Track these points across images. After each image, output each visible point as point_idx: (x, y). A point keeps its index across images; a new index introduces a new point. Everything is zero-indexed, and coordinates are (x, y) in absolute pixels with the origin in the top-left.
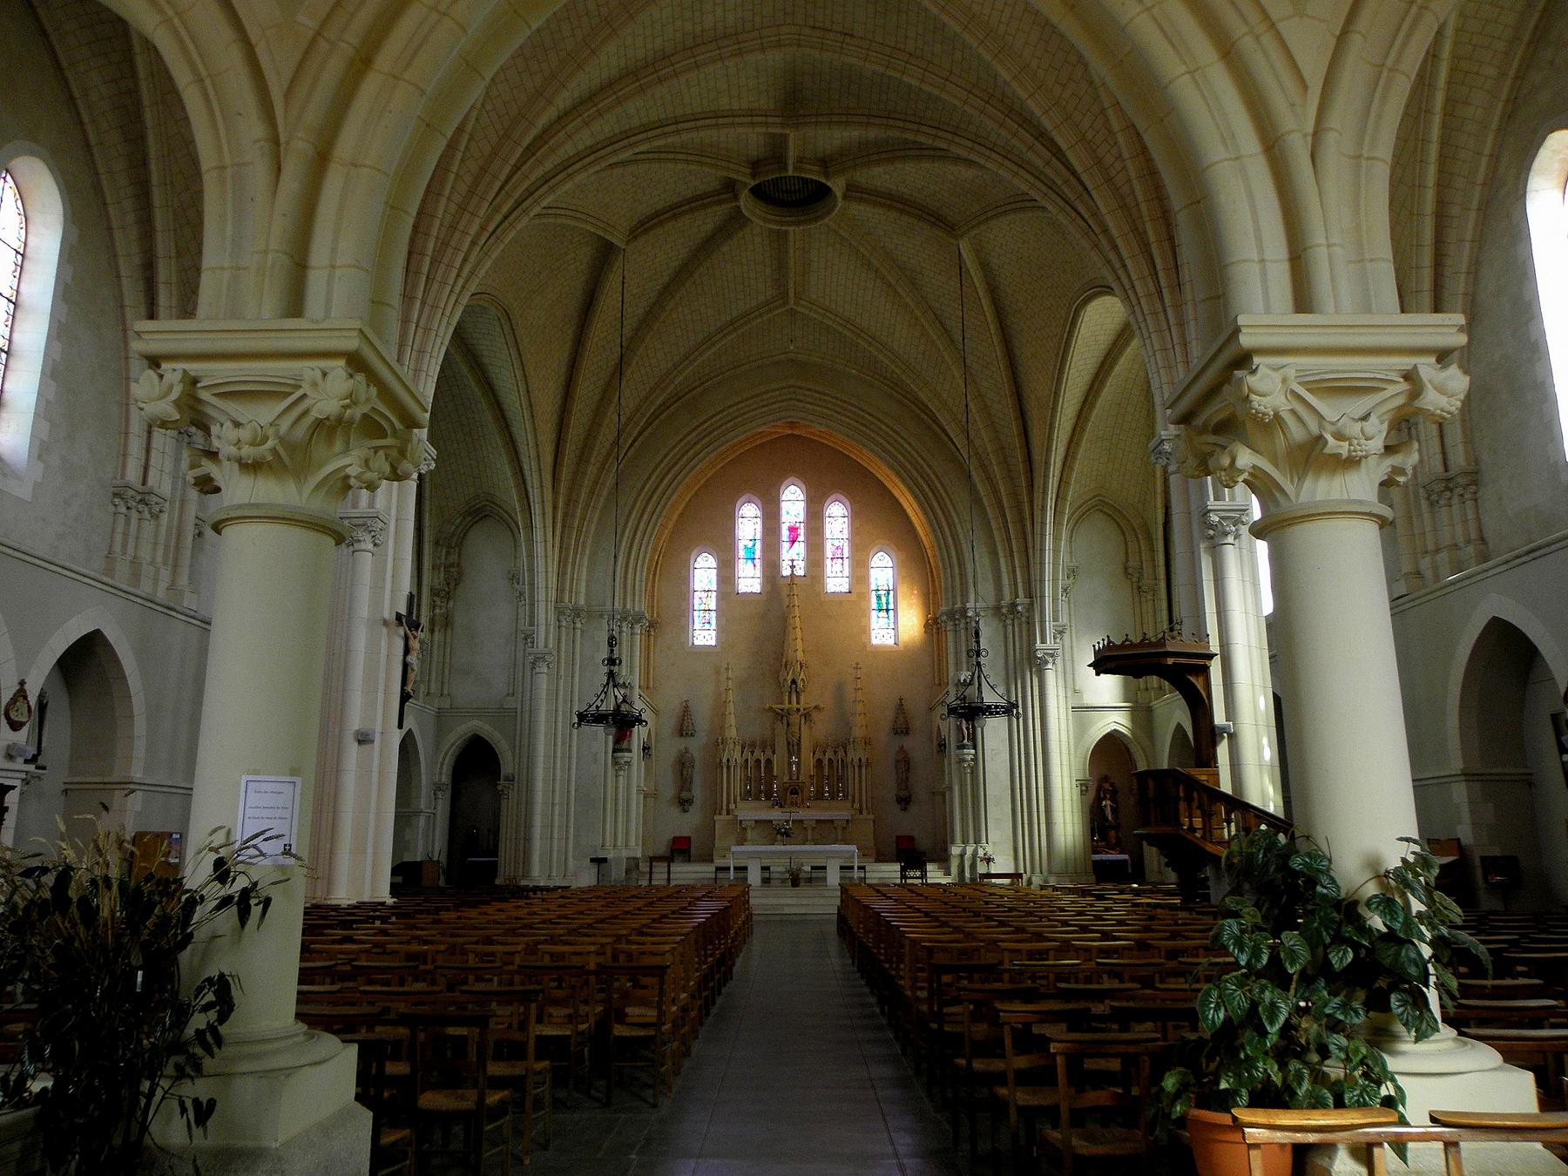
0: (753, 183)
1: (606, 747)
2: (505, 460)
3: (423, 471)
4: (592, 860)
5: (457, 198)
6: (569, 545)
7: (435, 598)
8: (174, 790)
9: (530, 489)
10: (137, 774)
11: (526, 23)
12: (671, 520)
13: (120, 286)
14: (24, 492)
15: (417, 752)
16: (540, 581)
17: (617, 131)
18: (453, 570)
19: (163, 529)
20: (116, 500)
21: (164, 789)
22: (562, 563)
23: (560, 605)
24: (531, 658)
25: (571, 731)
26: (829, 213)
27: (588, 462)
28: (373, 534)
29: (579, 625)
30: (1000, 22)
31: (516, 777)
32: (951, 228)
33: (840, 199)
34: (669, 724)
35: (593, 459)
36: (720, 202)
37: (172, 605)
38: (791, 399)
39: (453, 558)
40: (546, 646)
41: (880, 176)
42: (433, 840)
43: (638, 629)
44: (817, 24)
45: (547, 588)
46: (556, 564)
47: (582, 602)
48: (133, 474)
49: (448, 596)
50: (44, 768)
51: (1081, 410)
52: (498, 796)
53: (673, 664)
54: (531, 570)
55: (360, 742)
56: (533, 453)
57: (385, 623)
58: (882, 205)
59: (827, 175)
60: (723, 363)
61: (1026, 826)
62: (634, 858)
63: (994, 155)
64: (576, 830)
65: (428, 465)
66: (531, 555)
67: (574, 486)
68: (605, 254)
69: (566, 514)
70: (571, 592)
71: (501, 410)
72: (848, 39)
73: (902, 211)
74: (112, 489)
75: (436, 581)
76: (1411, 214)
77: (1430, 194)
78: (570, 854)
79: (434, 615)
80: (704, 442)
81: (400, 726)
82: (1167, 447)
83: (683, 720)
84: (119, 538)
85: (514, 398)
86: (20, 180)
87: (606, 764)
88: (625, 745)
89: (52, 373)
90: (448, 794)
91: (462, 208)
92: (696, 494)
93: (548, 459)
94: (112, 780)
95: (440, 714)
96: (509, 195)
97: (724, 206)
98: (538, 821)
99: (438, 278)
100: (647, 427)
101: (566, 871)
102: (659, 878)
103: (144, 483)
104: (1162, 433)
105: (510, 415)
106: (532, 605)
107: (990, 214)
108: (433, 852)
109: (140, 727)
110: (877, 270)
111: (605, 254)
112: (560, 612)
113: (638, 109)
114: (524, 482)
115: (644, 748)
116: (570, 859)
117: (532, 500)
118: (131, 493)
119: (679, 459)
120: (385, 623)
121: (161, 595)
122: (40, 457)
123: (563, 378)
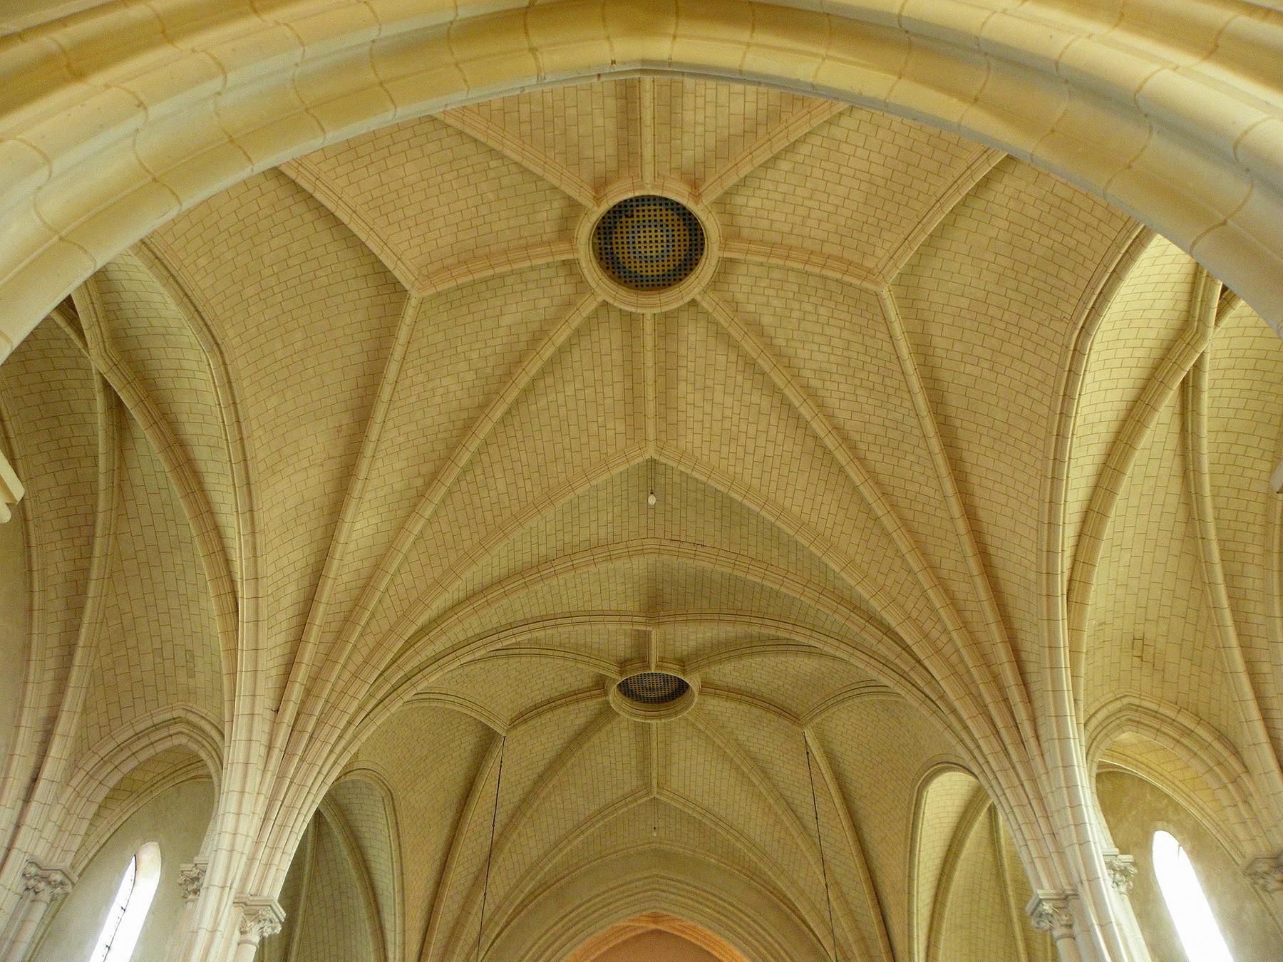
0: (621, 680)
2: (371, 947)
3: (266, 935)
5: (352, 667)
11: (320, 124)
12: (498, 925)
13: (16, 735)
17: (504, 623)
26: (687, 708)
30: (826, 527)
32: (796, 718)
33: (696, 694)
36: (591, 697)
38: (653, 889)
41: (728, 672)
44: (674, 538)
51: (936, 895)
56: (399, 940)
58: (733, 699)
59: (684, 672)
60: (592, 853)
63: (830, 641)
65: (273, 929)
68: (488, 740)
71: (375, 895)
72: (699, 548)
73: (751, 704)
76: (1224, 672)
77: (1237, 654)
82: (1047, 907)
85: (388, 881)
91: (355, 676)
96: (400, 668)
97: (595, 701)
99: (322, 737)
100: (514, 917)
104: (1039, 892)
107: (830, 703)
110: (732, 761)
111: (488, 740)
113: (522, 603)
119: (544, 951)
123: (438, 863)
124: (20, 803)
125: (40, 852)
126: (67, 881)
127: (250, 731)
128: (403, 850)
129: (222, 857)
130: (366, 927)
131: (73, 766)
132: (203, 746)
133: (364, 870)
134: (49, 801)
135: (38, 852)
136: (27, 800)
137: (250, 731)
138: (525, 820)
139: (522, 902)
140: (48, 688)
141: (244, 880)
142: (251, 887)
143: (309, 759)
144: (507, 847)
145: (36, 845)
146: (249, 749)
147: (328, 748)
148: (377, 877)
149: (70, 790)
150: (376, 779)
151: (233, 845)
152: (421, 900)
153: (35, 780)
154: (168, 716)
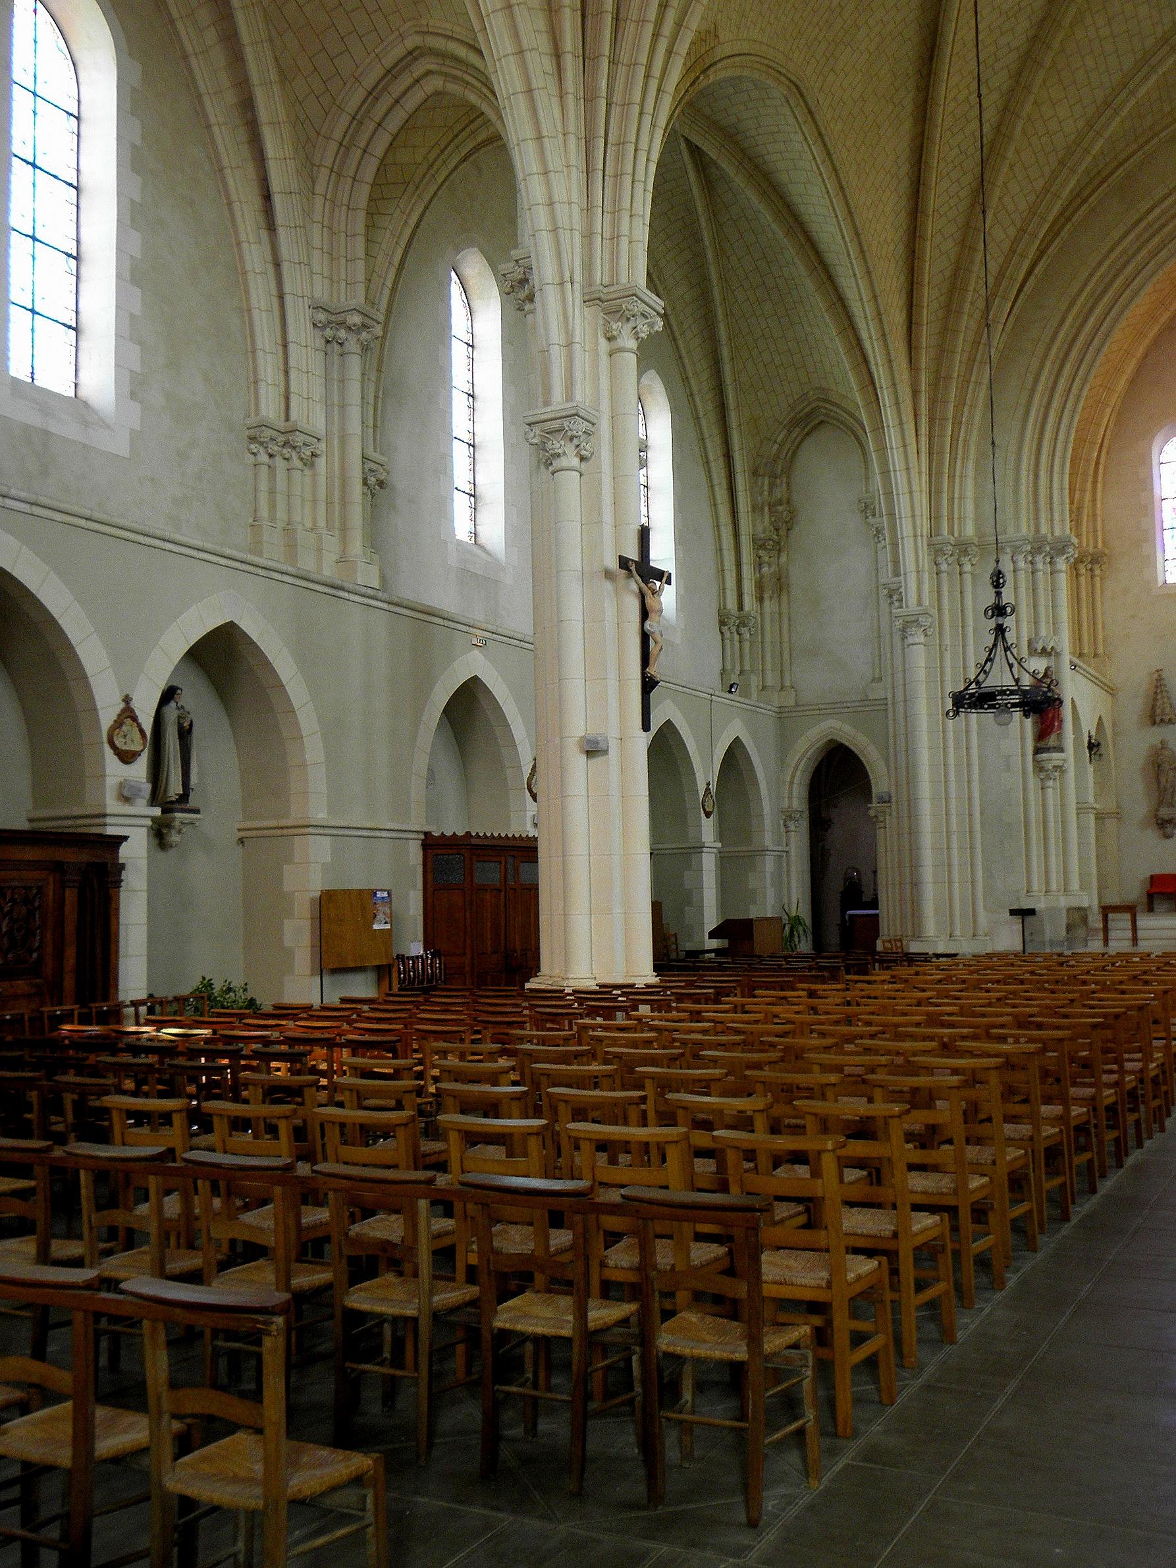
1: (1023, 747)
4: (1013, 912)
6: (942, 447)
7: (761, 553)
8: (378, 834)
9: (874, 369)
10: (320, 814)
14: (121, 446)
15: (752, 769)
16: (903, 506)
18: (780, 508)
19: (322, 480)
20: (252, 446)
21: (360, 833)
22: (934, 476)
23: (935, 540)
24: (899, 623)
25: (944, 724)
27: (959, 312)
28: (576, 441)
29: (967, 568)
31: (894, 799)
34: (1134, 707)
35: (967, 306)
37: (338, 582)
39: (780, 492)
40: (920, 603)
42: (789, 888)
43: (1062, 564)
45: (913, 516)
46: (925, 477)
47: (970, 530)
48: (270, 408)
49: (779, 548)
50: (197, 811)
52: (873, 822)
53: (1133, 617)
54: (889, 494)
55: (590, 754)
56: (869, 309)
57: (608, 575)
61: (452, 994)
62: (1079, 909)
64: (987, 870)
65: (651, 325)
66: (886, 473)
67: (943, 352)
69: (933, 402)
70: (951, 518)
71: (818, 253)
74: (247, 433)
75: (760, 529)
78: (980, 903)
79: (761, 577)
80: (1150, 246)
81: (646, 727)
83: (1155, 699)
84: (263, 498)
86: (53, 7)
87: (1024, 772)
88: (1052, 740)
89: (133, 275)
90: (805, 824)
92: (1156, 343)
93: (896, 316)
94: (290, 823)
95: (782, 714)
98: (928, 856)
101: (975, 928)
102: (1120, 942)
103: (287, 419)
105: (831, 258)
106: (895, 545)
108: (789, 903)
109: (314, 751)
112: (936, 551)
114: (866, 360)
115: (1091, 746)
116: (981, 912)
117: (878, 386)
118: (268, 433)
120: (608, 575)
121: (328, 571)
122: (133, 395)
123: (906, 183)
124: (264, 234)
125: (321, 291)
126: (370, 322)
127: (516, 35)
128: (841, 175)
129: (545, 240)
130: (819, 303)
131: (308, 166)
132: (468, 83)
133: (791, 220)
134: (299, 222)
135: (318, 294)
136: (271, 227)
137: (516, 35)
138: (1041, 74)
139: (1061, 214)
140: (219, 57)
141: (588, 267)
142: (600, 275)
143: (624, 57)
144: (1019, 129)
145: (312, 285)
146: (523, 65)
147: (649, 29)
148: (814, 228)
149: (319, 201)
150: (764, 68)
151: (553, 218)
152: (891, 247)
153: (267, 197)
154: (397, 52)
